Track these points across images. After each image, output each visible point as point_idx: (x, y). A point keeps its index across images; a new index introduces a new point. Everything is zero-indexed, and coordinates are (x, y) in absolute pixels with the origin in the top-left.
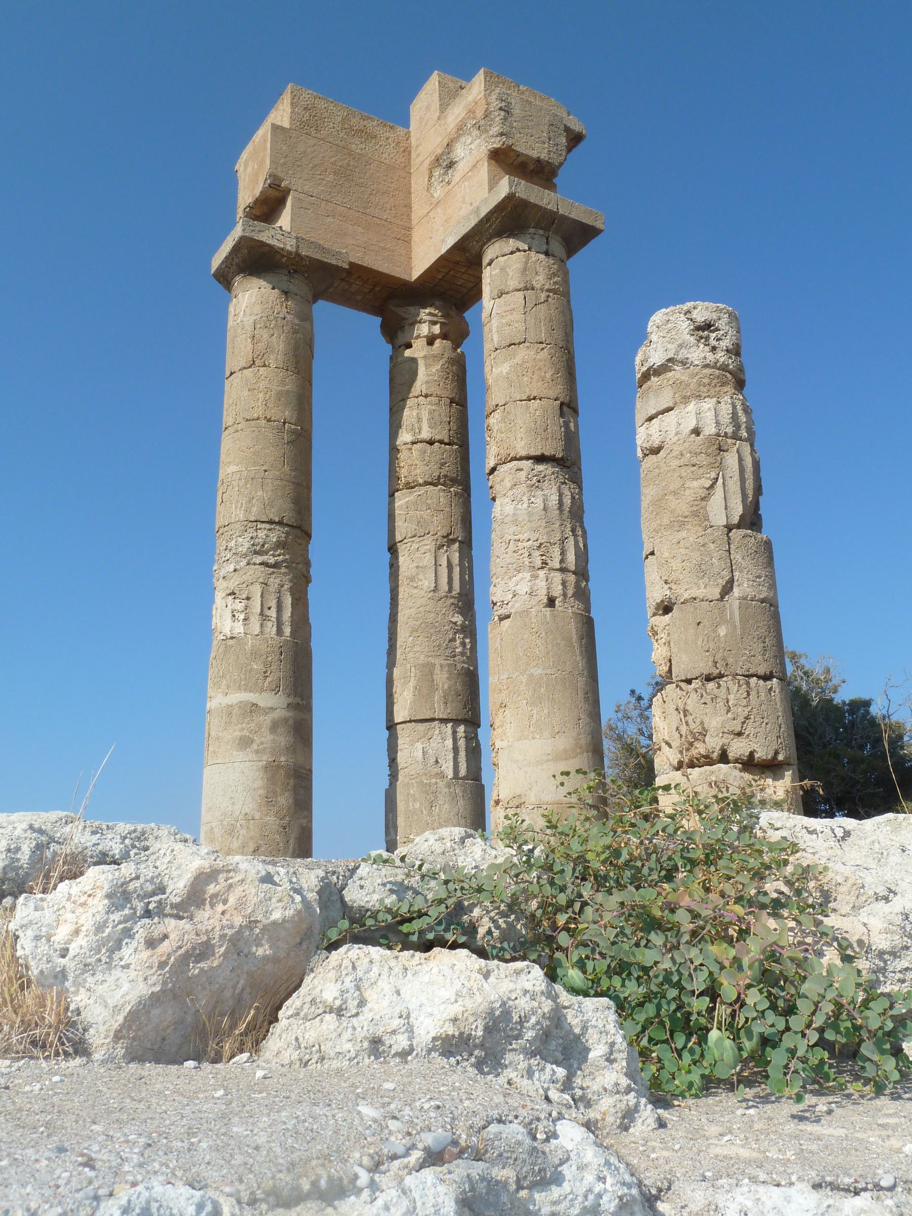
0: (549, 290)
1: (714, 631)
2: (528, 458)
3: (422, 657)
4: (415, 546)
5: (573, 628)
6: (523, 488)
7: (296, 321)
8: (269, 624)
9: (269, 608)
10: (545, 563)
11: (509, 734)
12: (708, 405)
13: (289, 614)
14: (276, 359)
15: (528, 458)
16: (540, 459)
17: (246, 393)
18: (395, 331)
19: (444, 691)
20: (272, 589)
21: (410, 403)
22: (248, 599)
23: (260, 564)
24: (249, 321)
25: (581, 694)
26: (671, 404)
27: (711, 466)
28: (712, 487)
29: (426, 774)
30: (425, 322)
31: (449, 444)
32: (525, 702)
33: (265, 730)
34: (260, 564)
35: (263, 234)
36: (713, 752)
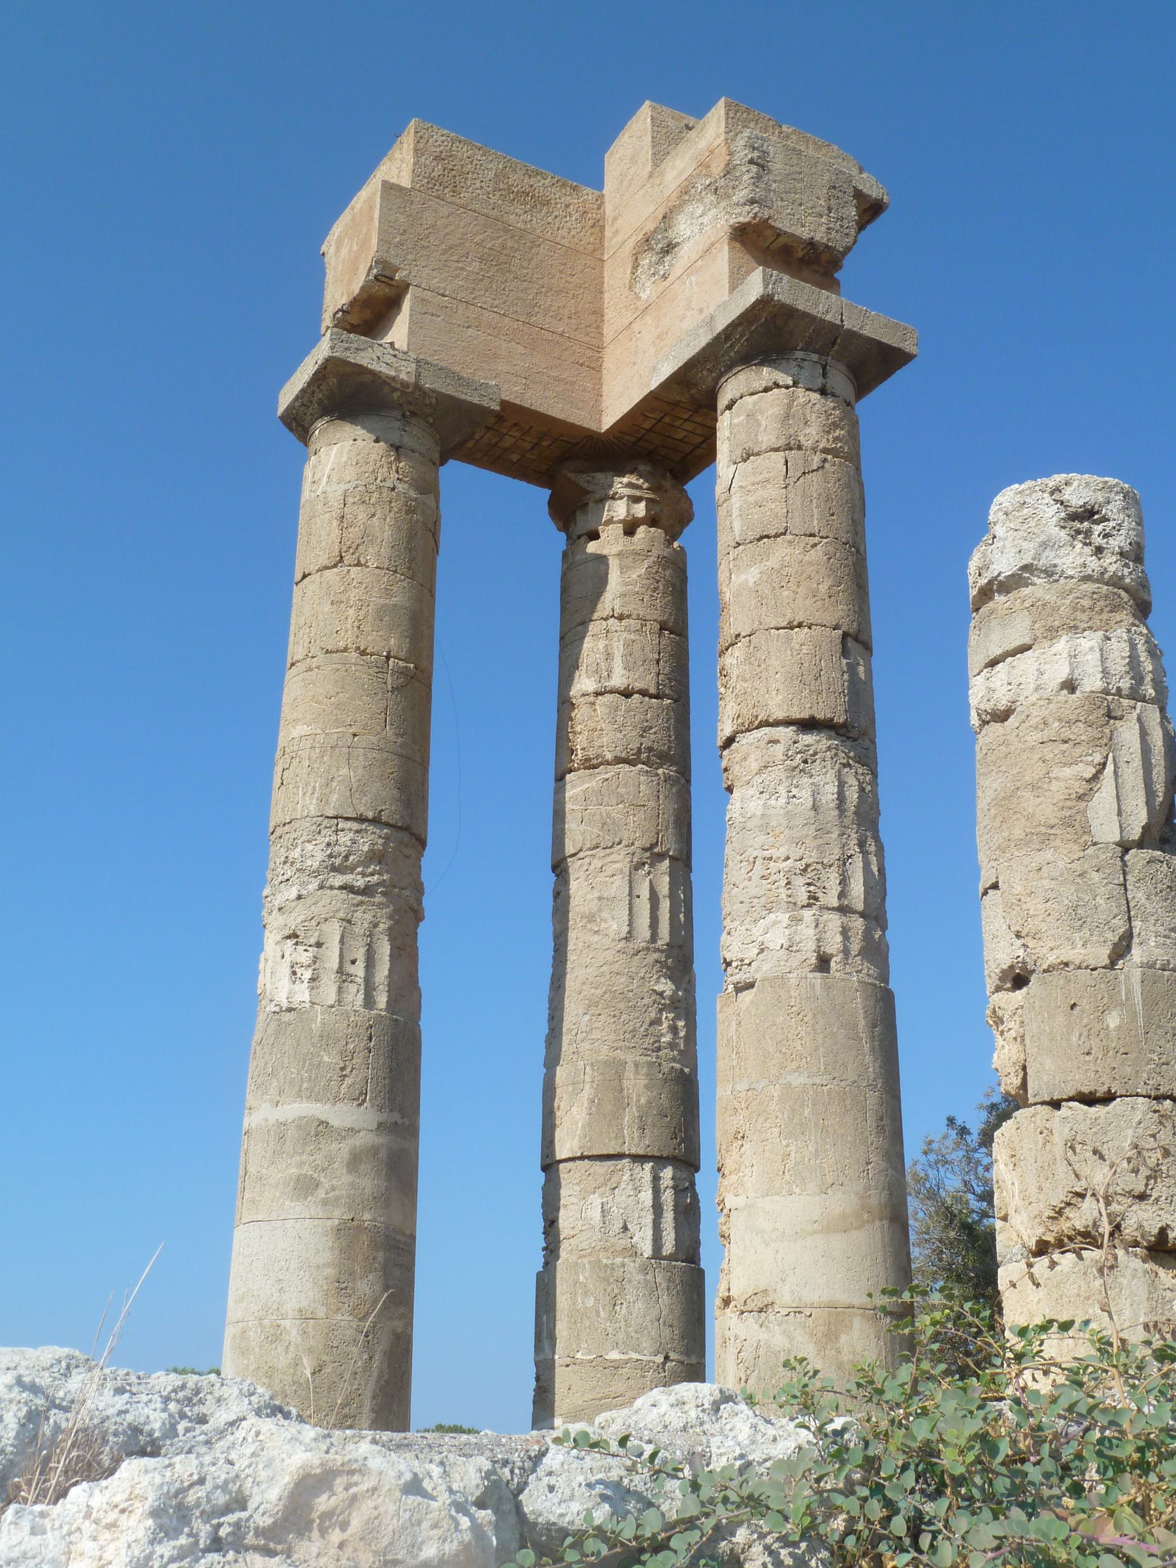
0: (825, 451)
1: (1100, 1020)
2: (788, 723)
4: (597, 863)
5: (858, 1007)
6: (778, 773)
8: (353, 988)
12: (1089, 642)
13: (386, 973)
14: (378, 554)
15: (788, 723)
16: (808, 725)
17: (327, 608)
18: (572, 511)
19: (639, 1108)
20: (359, 930)
21: (593, 628)
22: (319, 945)
23: (341, 888)
24: (336, 492)
25: (871, 1121)
26: (1027, 640)
27: (1095, 743)
28: (1095, 778)
29: (606, 1249)
30: (621, 498)
31: (657, 697)
32: (777, 1130)
33: (339, 1166)
34: (341, 888)
35: (363, 354)
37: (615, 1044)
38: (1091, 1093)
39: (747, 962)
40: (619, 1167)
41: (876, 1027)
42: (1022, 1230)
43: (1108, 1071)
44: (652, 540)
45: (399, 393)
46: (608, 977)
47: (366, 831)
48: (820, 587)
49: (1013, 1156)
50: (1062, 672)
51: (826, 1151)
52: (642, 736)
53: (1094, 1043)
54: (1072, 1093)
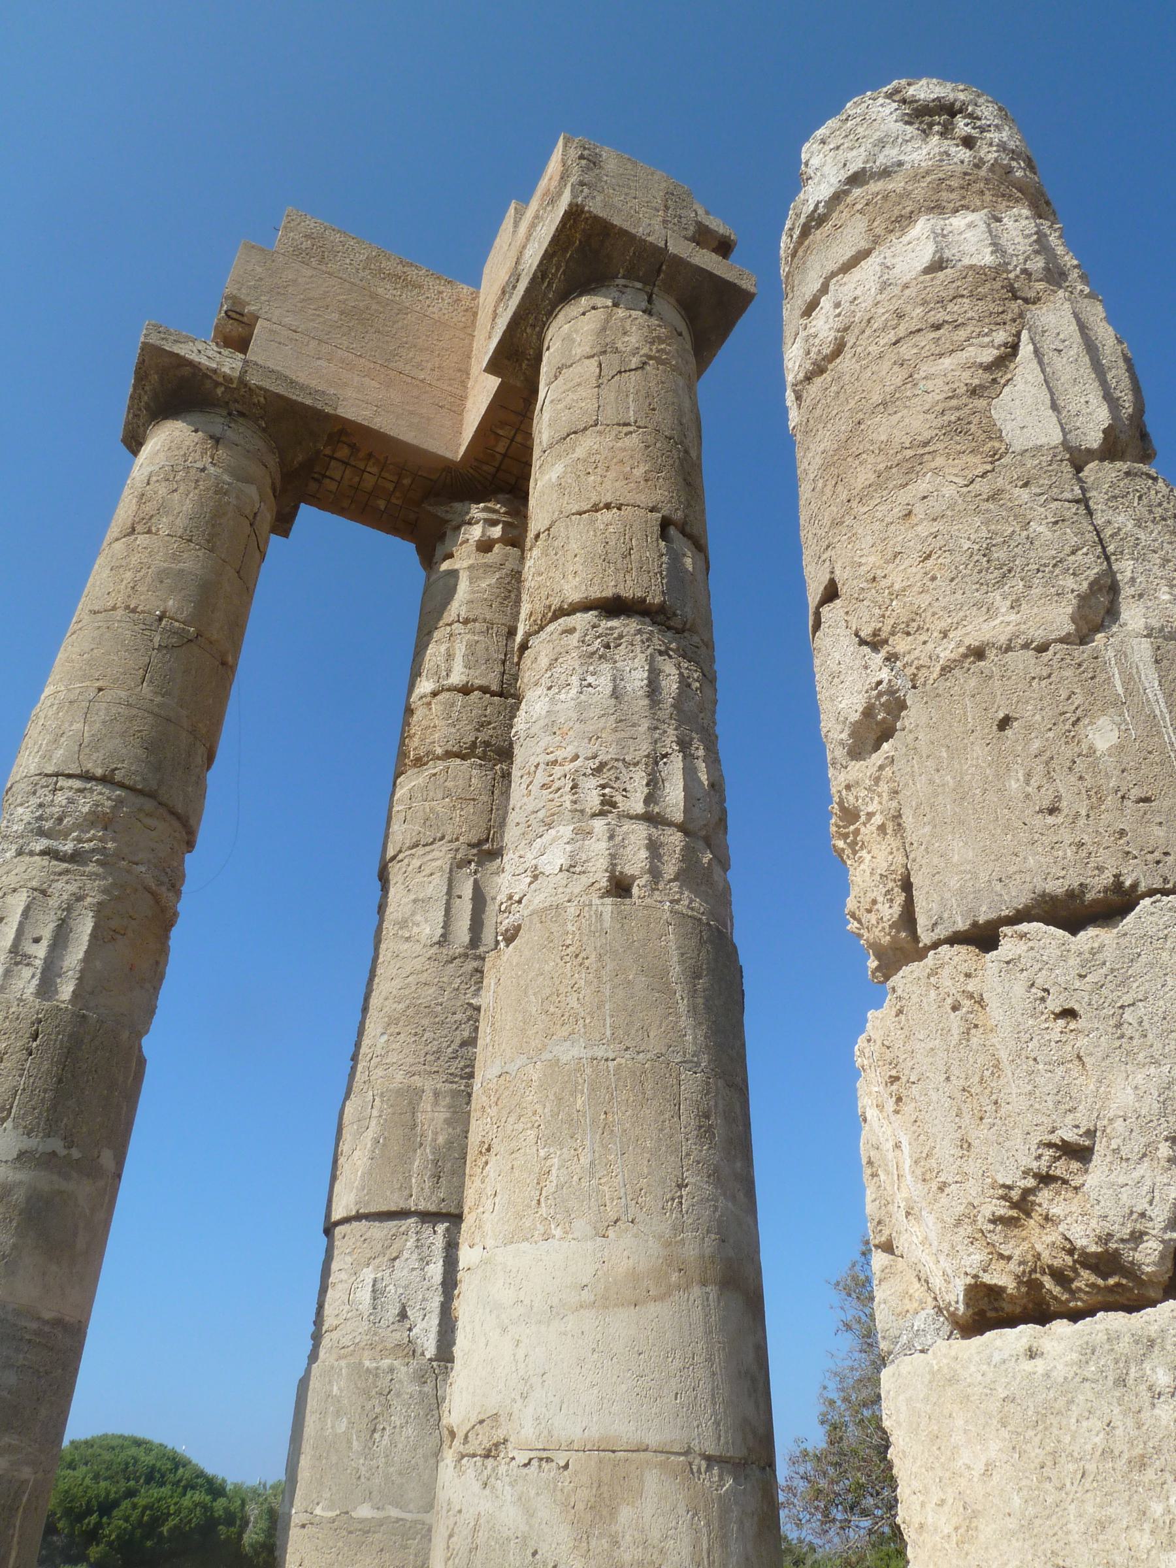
1: (1070, 738)
3: (400, 1076)
4: (416, 863)
5: (672, 950)
6: (572, 661)
7: (226, 478)
8: (27, 972)
9: (37, 940)
10: (608, 803)
11: (487, 1227)
13: (81, 955)
14: (172, 524)
15: (585, 606)
16: (613, 607)
18: (431, 541)
19: (436, 1150)
21: (437, 635)
23: (43, 853)
25: (688, 1118)
26: (864, 245)
29: (372, 1346)
30: (477, 522)
31: (501, 695)
32: (531, 1134)
34: (43, 853)
36: (1137, 1237)
37: (413, 1069)
38: (1071, 895)
39: (516, 898)
40: (403, 1229)
41: (699, 977)
42: (927, 1259)
43: (1107, 840)
44: (507, 555)
45: (223, 389)
46: (414, 988)
47: (91, 790)
48: (635, 471)
49: (895, 1079)
50: (926, 254)
51: (609, 1164)
52: (478, 730)
53: (1065, 785)
54: (1022, 899)
